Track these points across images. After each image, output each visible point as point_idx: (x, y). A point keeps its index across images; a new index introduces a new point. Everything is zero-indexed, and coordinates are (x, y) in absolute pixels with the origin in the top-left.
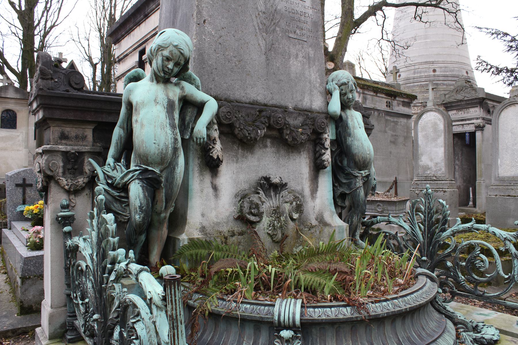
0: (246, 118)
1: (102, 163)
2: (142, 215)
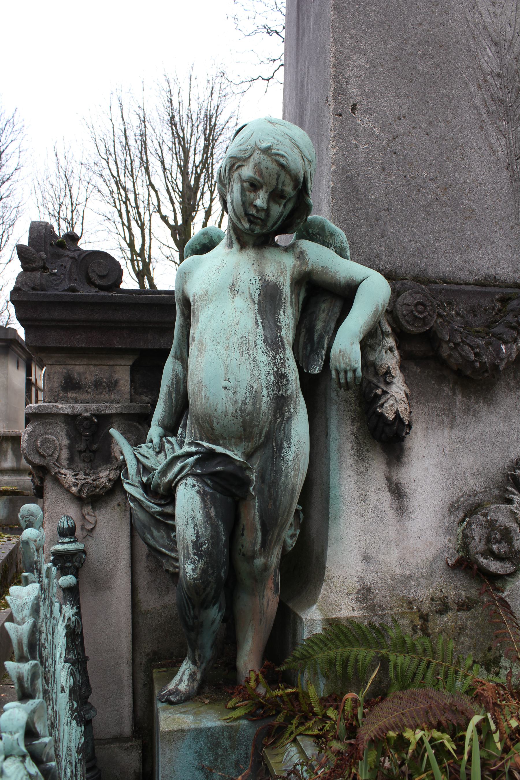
0: (470, 318)
1: (137, 439)
2: (200, 565)
